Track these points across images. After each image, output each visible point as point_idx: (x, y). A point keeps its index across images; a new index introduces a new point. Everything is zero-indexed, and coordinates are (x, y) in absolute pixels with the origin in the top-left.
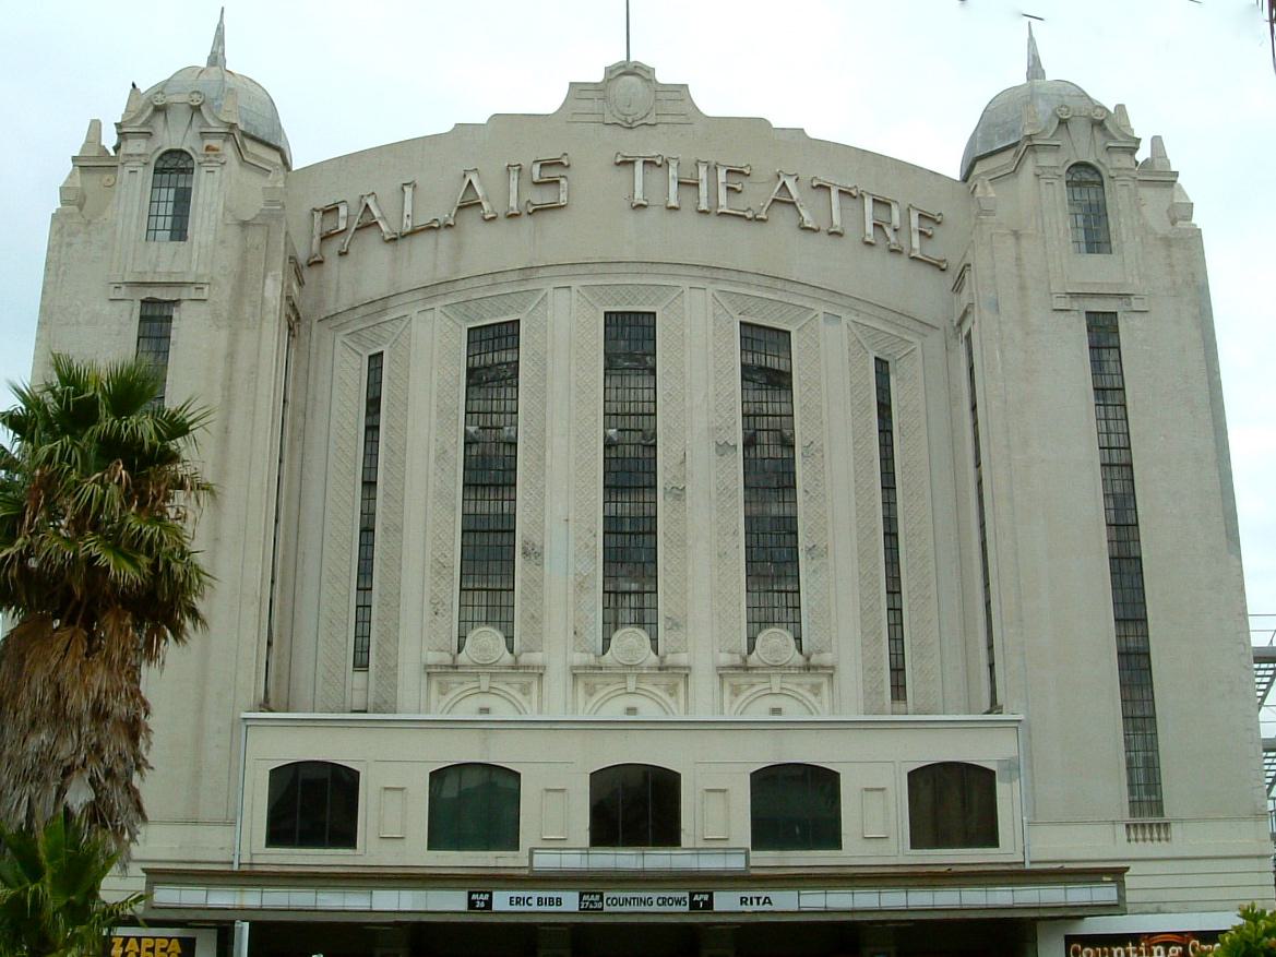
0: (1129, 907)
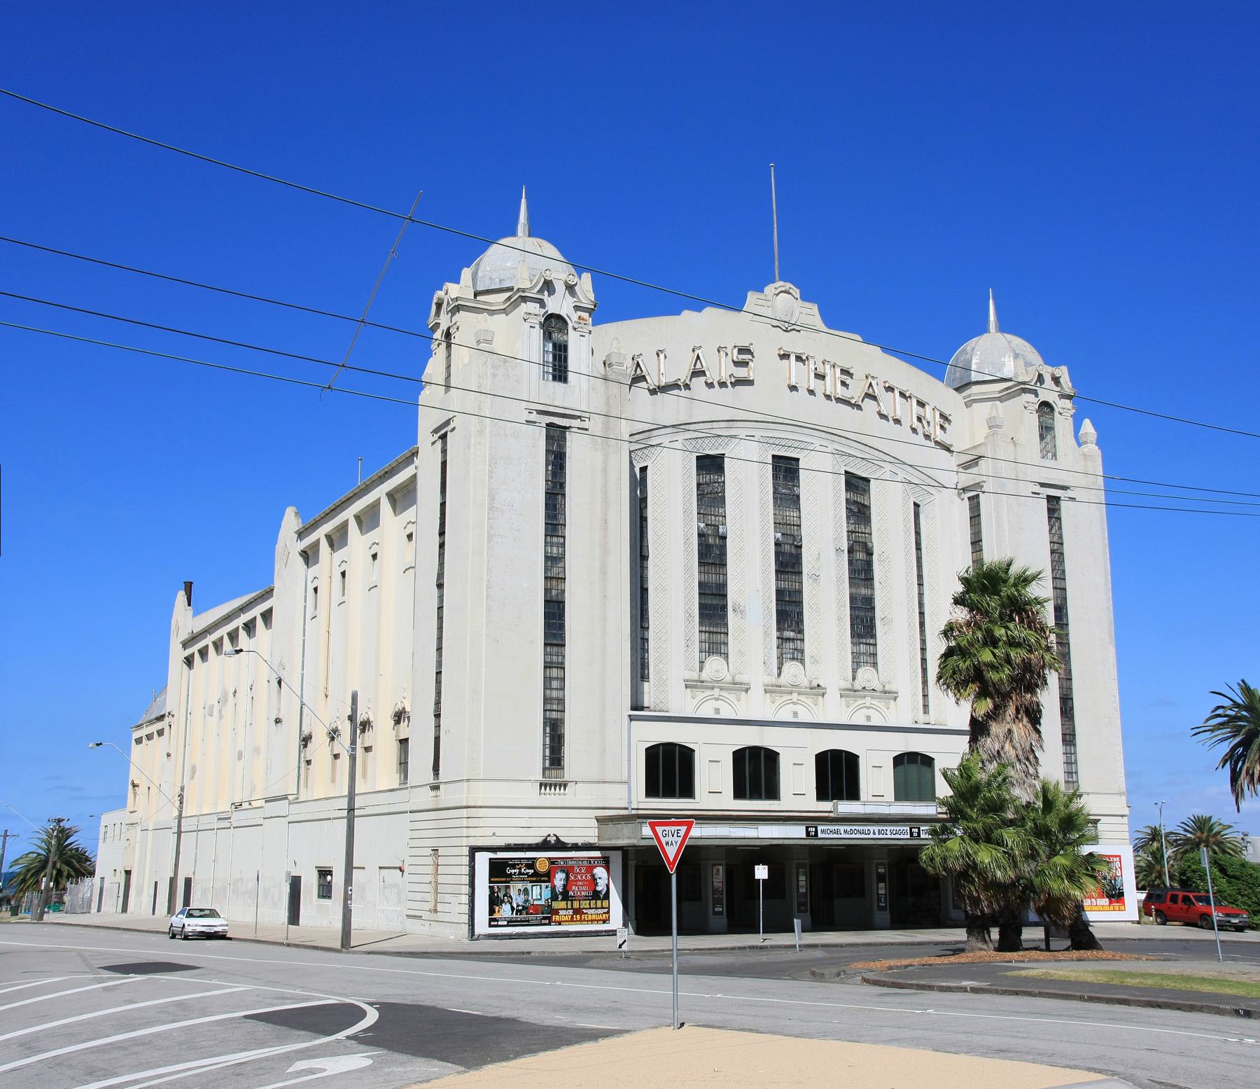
0: (1025, 945)
